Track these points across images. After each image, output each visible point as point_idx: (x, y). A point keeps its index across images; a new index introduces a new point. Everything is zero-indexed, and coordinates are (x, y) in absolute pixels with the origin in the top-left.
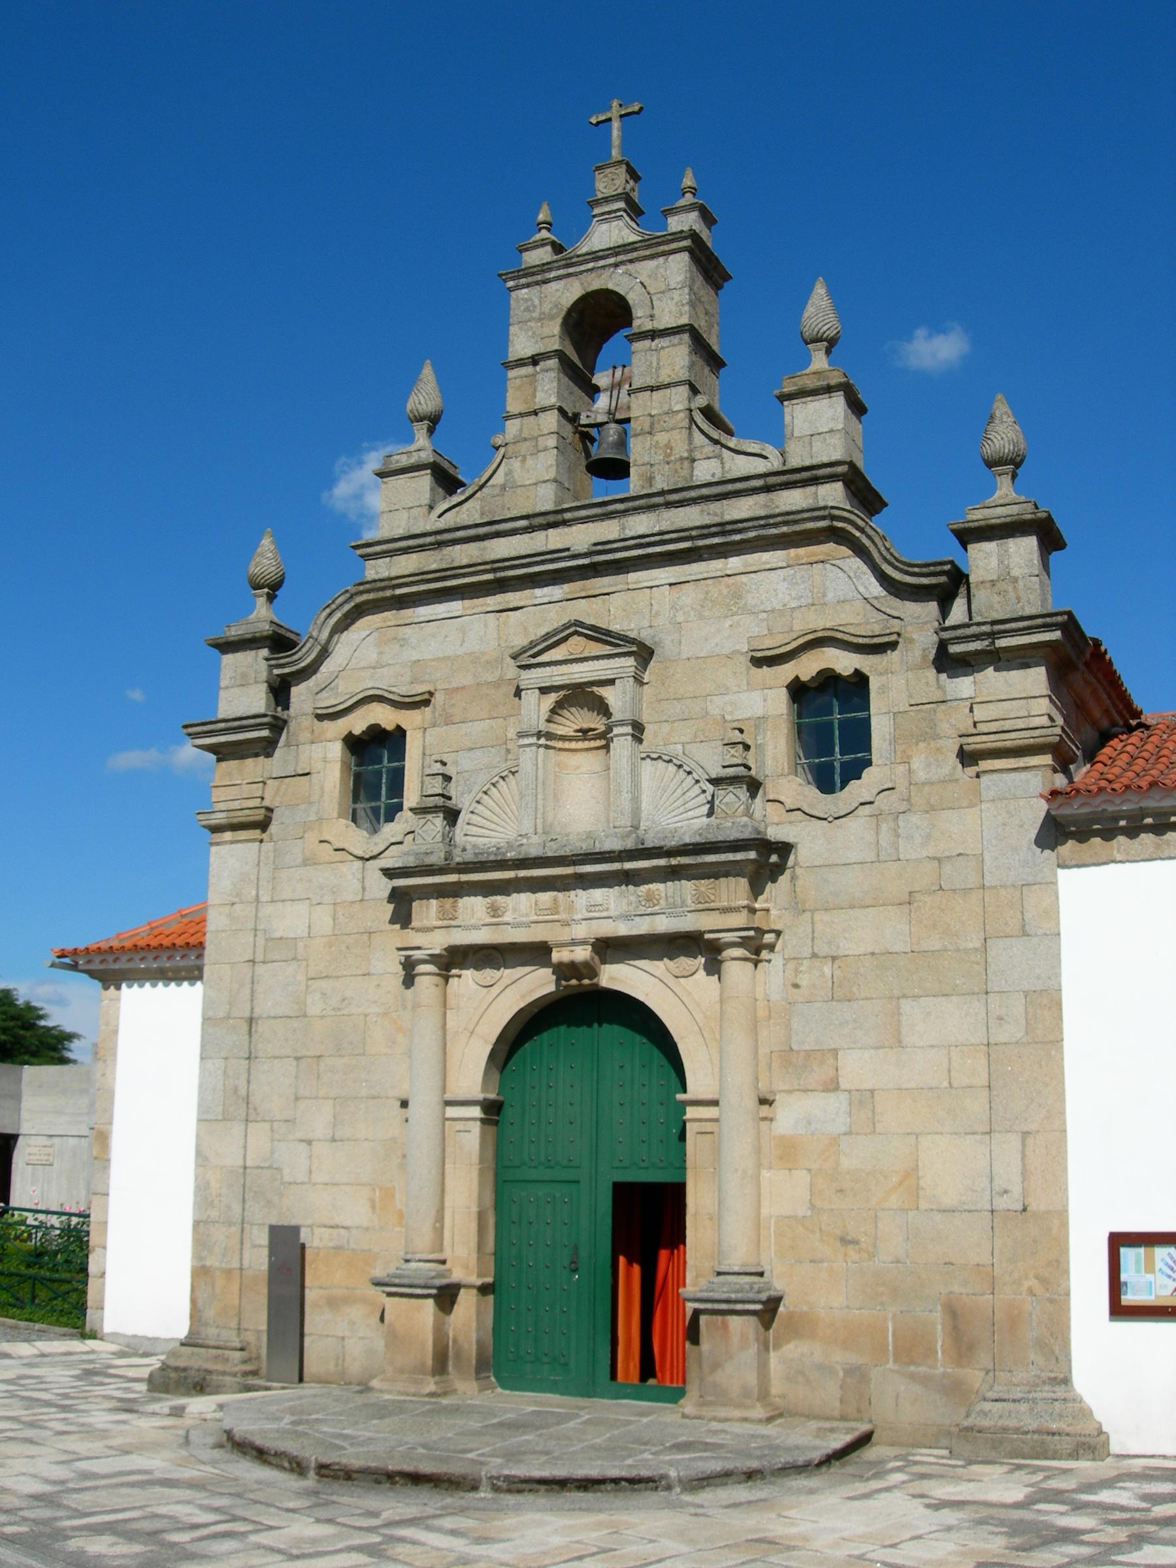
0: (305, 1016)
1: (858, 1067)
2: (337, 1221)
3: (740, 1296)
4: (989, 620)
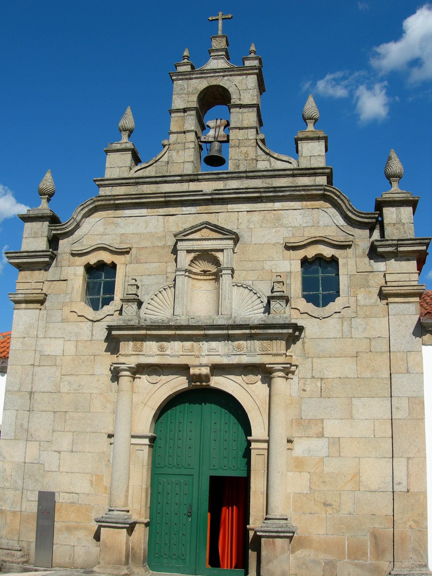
0: (60, 392)
1: (332, 427)
2: (72, 490)
3: (283, 529)
4: (397, 239)
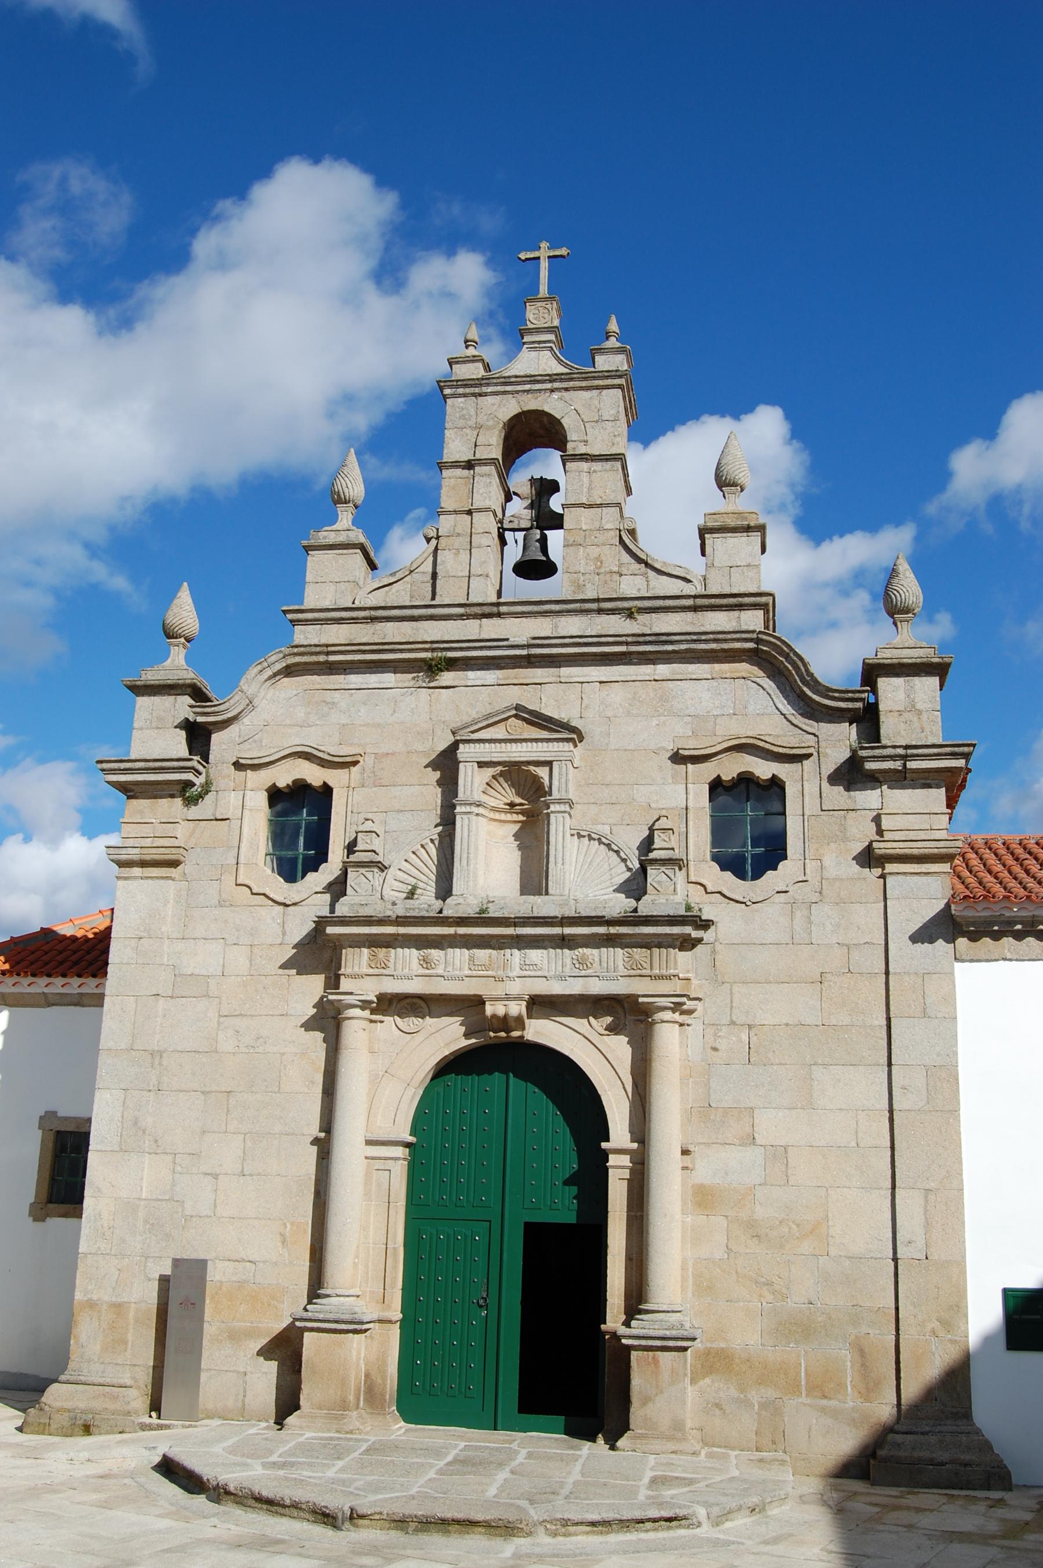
0: (217, 1052)
1: (772, 1125)
